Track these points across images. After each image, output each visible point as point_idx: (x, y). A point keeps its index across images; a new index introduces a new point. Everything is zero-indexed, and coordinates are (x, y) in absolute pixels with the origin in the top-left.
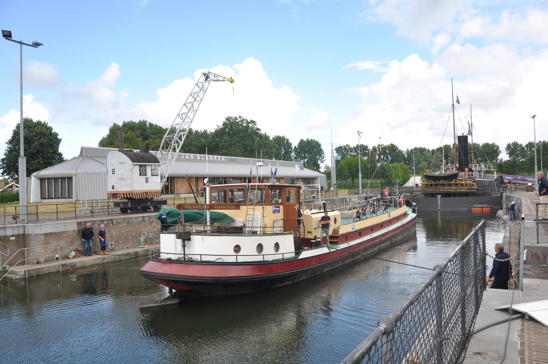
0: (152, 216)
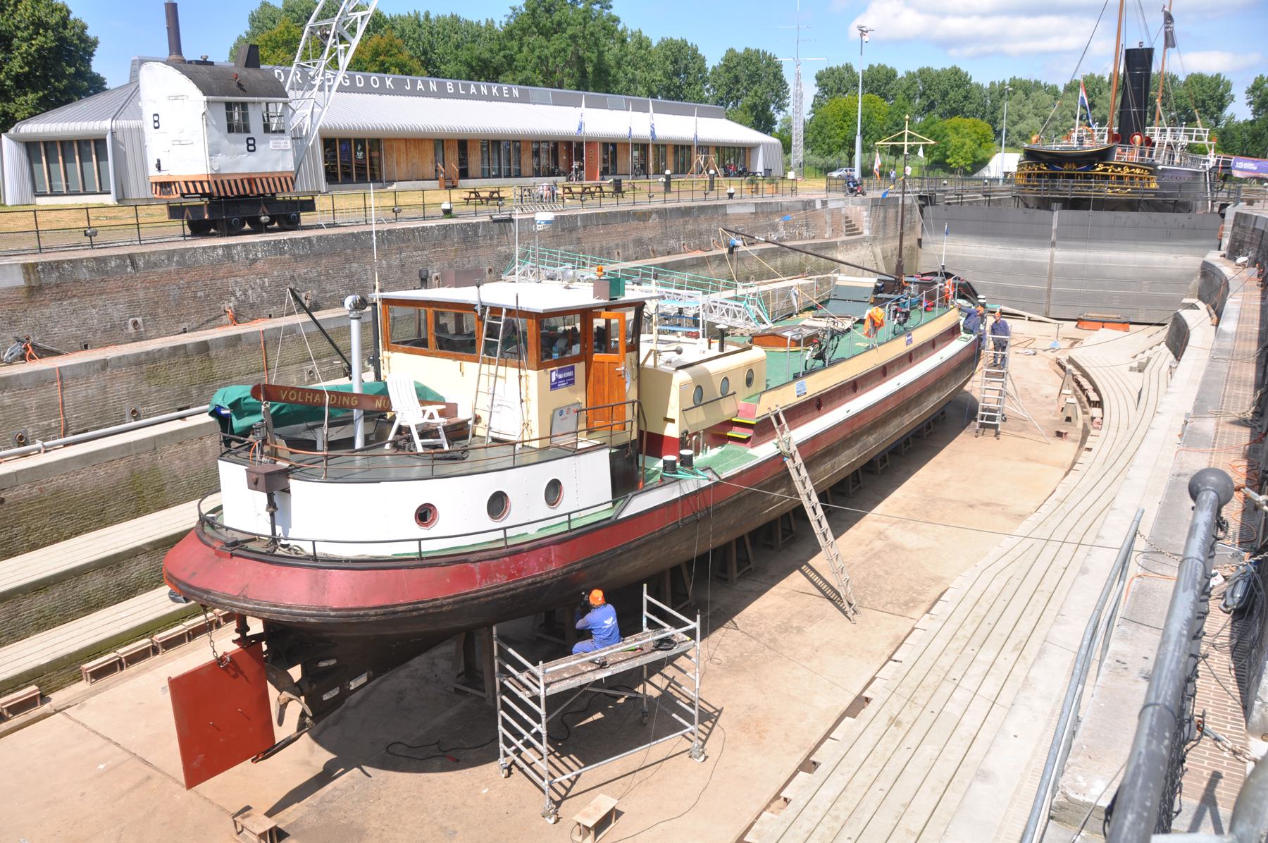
0: (254, 244)
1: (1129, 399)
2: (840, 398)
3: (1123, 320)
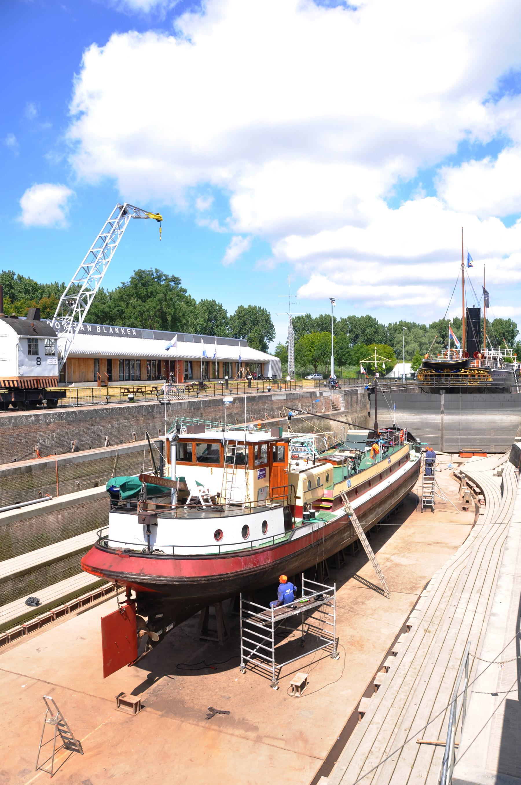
0: (49, 414)
1: (496, 489)
2: (364, 489)
3: (483, 451)
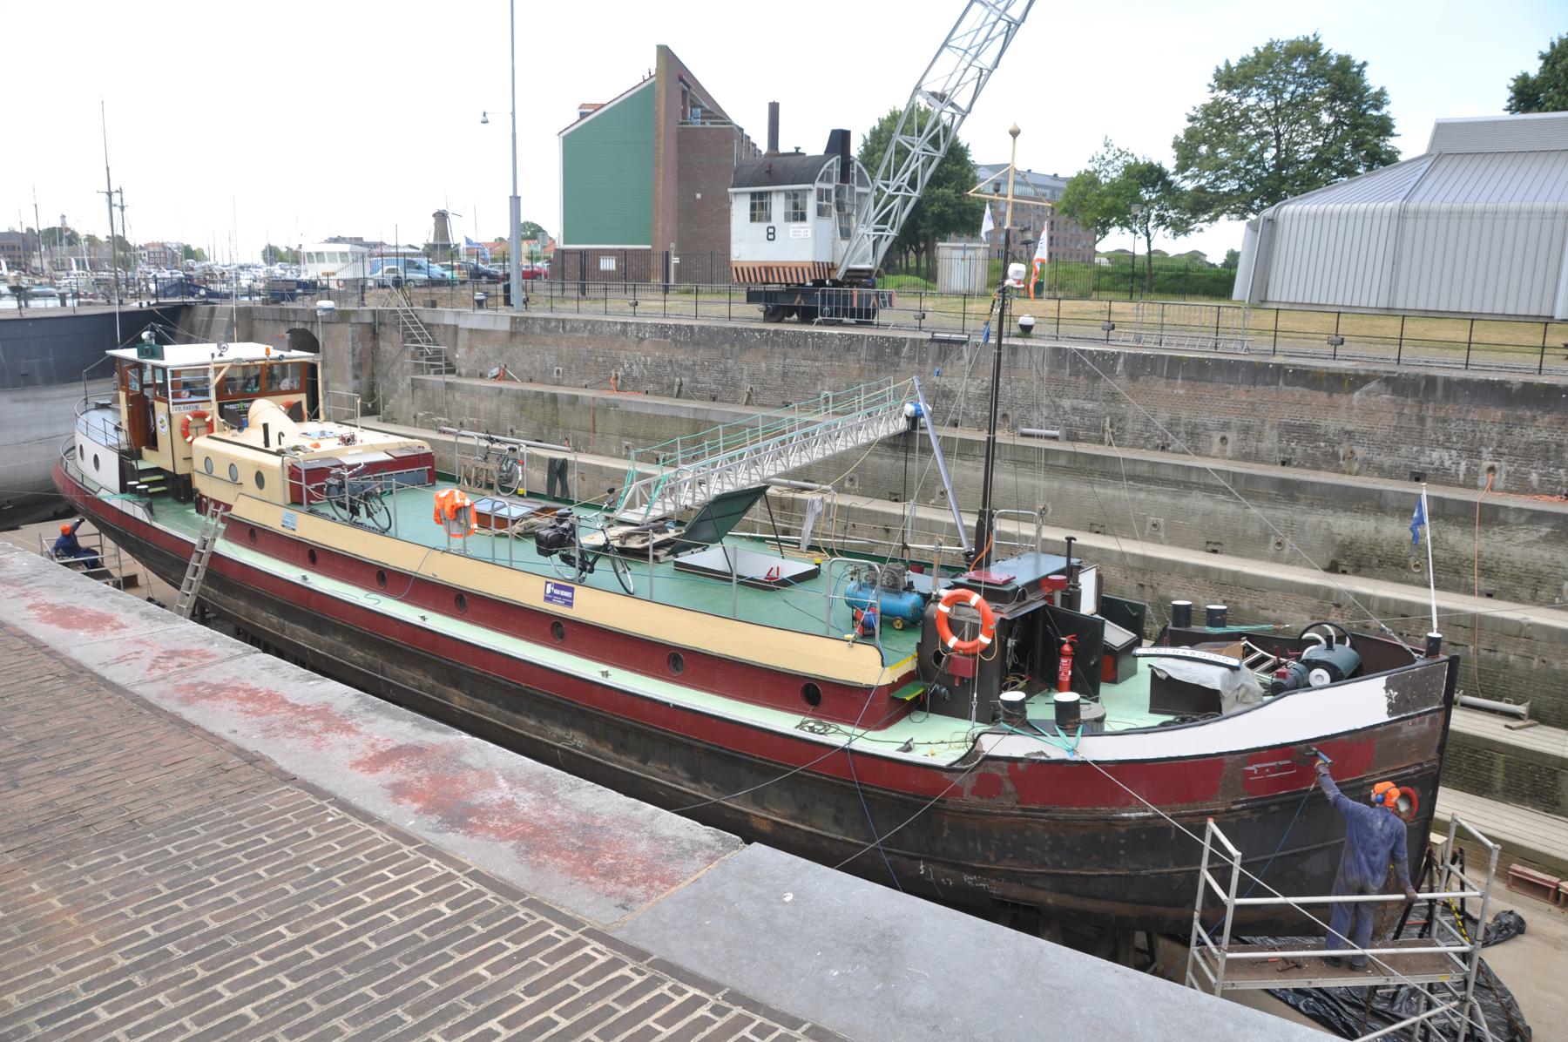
0: (645, 325)
